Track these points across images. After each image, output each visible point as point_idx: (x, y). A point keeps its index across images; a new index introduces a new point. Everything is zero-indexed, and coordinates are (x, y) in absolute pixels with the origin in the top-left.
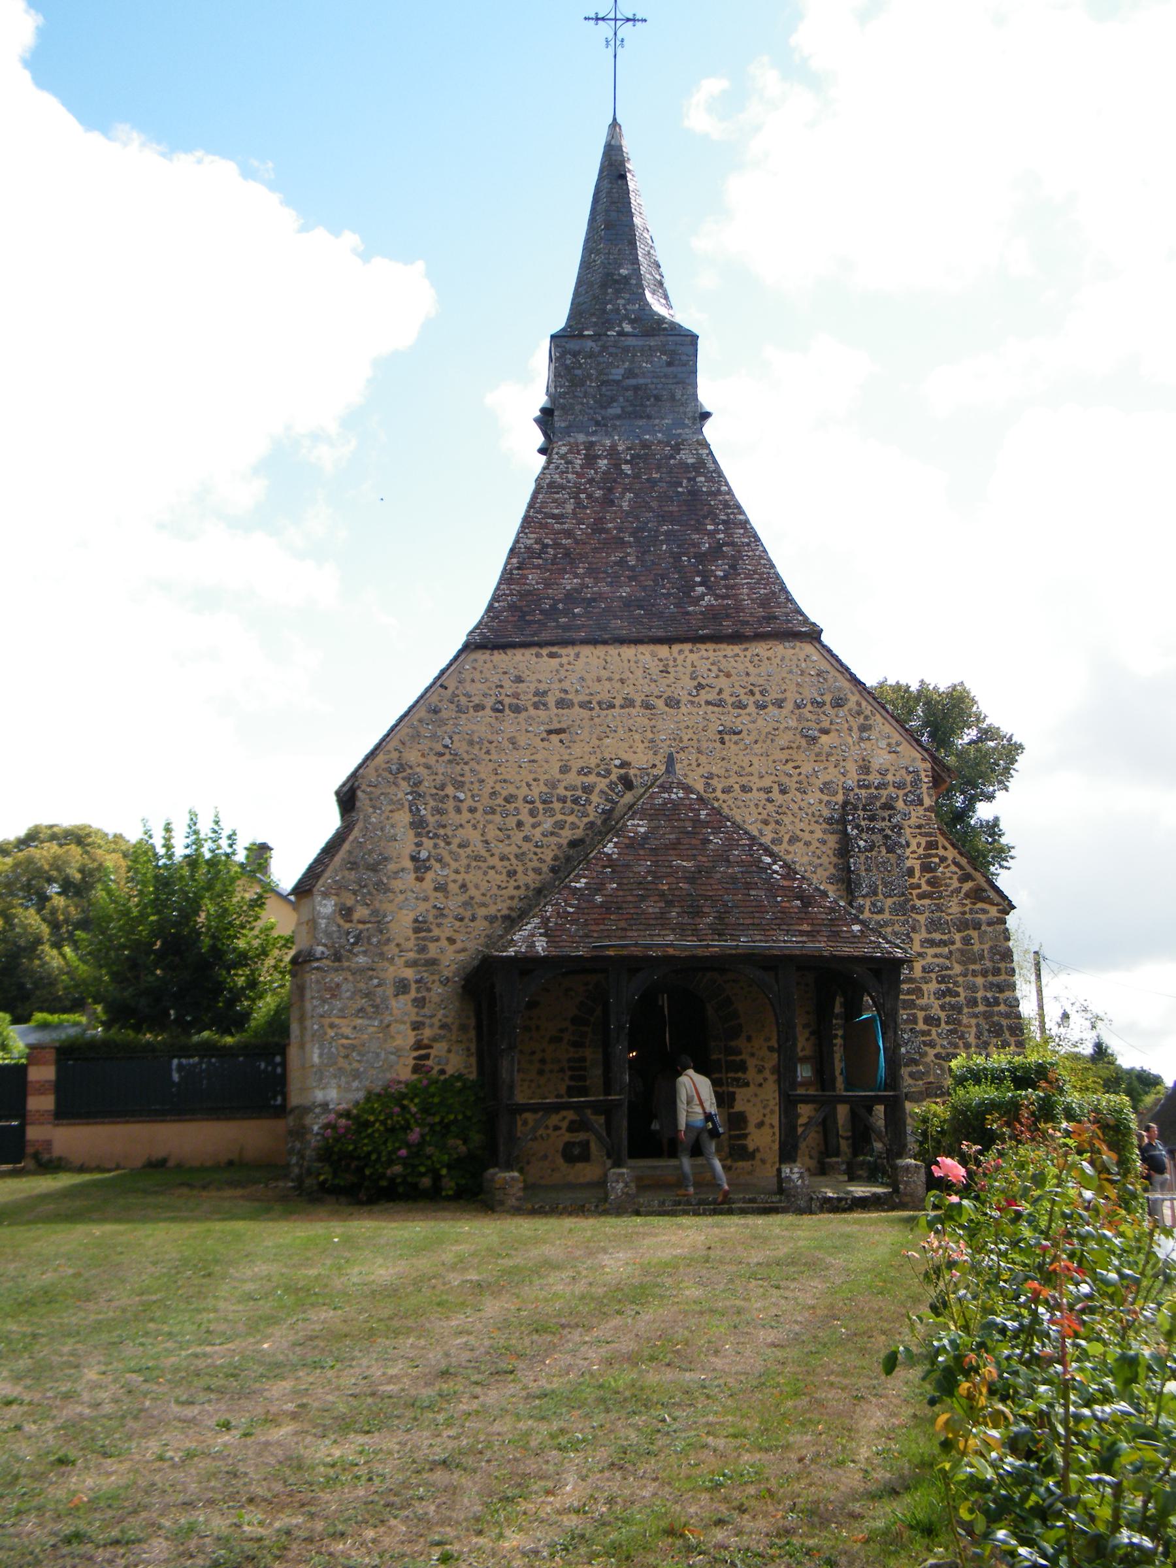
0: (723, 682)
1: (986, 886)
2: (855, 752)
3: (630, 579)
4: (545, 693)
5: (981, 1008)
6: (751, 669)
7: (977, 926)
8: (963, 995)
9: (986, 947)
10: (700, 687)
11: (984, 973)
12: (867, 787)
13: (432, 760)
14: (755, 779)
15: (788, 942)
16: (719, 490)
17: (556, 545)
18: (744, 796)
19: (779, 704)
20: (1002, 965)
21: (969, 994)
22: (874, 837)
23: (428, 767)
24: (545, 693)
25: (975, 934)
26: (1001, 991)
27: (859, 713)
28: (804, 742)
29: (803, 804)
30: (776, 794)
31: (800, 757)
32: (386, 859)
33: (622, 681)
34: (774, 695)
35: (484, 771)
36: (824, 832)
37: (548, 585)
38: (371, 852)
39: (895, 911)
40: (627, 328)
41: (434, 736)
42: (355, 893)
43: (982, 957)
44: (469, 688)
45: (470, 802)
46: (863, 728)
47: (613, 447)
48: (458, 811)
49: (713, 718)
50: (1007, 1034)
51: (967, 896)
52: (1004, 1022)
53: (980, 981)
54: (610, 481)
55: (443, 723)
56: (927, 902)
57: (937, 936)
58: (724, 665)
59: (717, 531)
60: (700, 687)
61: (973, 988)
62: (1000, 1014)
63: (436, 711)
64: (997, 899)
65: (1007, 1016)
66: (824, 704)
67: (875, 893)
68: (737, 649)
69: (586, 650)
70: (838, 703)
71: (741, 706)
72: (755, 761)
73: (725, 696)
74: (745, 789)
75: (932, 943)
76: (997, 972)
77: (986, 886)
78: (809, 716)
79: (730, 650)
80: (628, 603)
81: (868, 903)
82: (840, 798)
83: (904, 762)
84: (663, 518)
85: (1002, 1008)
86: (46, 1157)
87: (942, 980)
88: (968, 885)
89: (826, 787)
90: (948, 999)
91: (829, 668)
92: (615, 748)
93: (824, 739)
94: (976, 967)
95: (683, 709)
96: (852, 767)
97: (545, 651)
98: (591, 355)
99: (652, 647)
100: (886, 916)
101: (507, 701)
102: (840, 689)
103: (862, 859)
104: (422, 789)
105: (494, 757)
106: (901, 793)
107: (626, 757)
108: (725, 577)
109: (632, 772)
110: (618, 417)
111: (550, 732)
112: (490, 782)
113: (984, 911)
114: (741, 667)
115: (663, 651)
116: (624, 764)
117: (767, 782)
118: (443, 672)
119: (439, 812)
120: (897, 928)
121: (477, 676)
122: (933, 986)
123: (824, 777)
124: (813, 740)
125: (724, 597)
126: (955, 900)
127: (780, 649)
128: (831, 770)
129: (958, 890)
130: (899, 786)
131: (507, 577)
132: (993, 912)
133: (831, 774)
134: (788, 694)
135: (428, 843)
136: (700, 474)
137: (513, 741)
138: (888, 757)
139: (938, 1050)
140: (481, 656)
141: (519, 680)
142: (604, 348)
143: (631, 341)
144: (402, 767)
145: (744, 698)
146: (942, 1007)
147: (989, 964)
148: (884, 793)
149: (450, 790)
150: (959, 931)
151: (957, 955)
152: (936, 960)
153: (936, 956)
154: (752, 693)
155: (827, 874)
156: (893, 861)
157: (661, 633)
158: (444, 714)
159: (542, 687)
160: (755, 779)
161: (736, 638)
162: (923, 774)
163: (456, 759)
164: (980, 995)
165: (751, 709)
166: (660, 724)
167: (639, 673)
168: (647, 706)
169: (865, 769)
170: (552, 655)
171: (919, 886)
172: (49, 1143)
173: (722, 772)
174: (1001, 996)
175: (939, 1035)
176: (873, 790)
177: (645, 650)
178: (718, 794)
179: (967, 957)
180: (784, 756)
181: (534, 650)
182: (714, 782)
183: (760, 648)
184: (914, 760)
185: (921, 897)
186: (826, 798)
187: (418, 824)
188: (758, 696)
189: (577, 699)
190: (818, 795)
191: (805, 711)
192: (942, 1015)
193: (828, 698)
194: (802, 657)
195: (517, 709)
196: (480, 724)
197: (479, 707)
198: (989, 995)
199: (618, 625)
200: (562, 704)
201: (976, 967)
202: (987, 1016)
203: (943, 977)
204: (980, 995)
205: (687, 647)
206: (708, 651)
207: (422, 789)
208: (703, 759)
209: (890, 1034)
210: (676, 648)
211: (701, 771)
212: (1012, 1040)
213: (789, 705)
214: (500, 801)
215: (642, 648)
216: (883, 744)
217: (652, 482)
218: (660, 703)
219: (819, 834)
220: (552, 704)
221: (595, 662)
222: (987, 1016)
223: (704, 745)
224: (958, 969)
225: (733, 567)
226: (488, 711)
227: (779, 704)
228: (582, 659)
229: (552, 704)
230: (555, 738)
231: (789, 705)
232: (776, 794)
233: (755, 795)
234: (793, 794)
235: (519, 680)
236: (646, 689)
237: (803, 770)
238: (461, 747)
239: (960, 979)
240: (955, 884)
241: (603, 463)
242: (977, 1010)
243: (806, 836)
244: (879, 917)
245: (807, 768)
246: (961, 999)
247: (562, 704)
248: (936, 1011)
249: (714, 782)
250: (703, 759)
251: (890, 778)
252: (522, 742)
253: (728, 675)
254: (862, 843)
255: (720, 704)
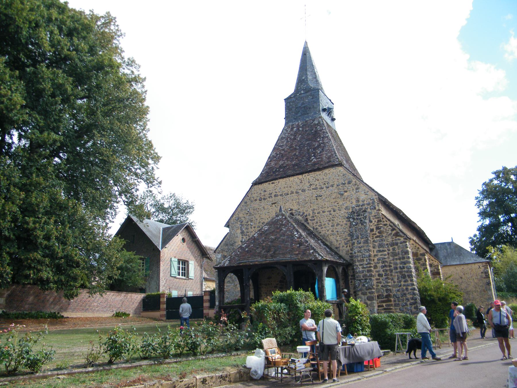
0: (317, 182)
1: (399, 231)
2: (355, 196)
3: (296, 158)
4: (271, 194)
5: (399, 270)
6: (324, 177)
7: (397, 244)
8: (393, 266)
9: (400, 251)
10: (311, 185)
11: (400, 259)
12: (359, 206)
13: (245, 215)
14: (326, 208)
15: (288, 257)
16: (323, 129)
17: (280, 153)
18: (324, 214)
19: (332, 186)
20: (405, 256)
21: (395, 266)
22: (358, 221)
23: (244, 217)
24: (271, 194)
25: (396, 247)
26: (405, 264)
27: (355, 185)
28: (339, 196)
29: (340, 214)
30: (332, 212)
31: (338, 200)
32: (235, 242)
33: (290, 187)
34: (331, 184)
35: (257, 216)
36: (346, 221)
37: (276, 165)
38: (231, 241)
39: (364, 243)
40: (302, 92)
41: (246, 209)
42: (227, 252)
43: (399, 254)
44: (253, 195)
45: (254, 225)
46: (357, 189)
47: (298, 124)
48: (251, 228)
49: (314, 193)
50: (407, 278)
51: (394, 235)
52: (406, 274)
53: (398, 261)
54: (295, 135)
55: (247, 205)
56: (378, 239)
57: (381, 249)
58: (317, 177)
59: (320, 140)
60: (311, 185)
61: (396, 264)
62: (405, 271)
63: (246, 203)
64: (403, 235)
65: (407, 272)
66: (345, 183)
67: (358, 238)
68: (320, 172)
69: (281, 180)
70: (349, 183)
71: (322, 188)
72: (326, 203)
73: (318, 186)
74: (324, 212)
75: (380, 251)
76: (404, 258)
77: (399, 231)
78: (341, 188)
79: (318, 173)
80: (294, 165)
81: (356, 241)
82: (351, 210)
83: (369, 197)
84: (307, 140)
85: (406, 269)
86: (207, 317)
87: (383, 262)
88: (394, 232)
89: (347, 208)
90: (385, 268)
91: (346, 173)
92: (289, 206)
93: (346, 194)
94: (397, 257)
95: (306, 192)
96: (354, 201)
97: (271, 183)
98: (293, 102)
99: (297, 176)
100: (362, 245)
101: (262, 197)
102: (350, 178)
103: (354, 228)
104: (243, 223)
105: (259, 212)
106: (369, 206)
107: (292, 208)
108: (320, 153)
109: (293, 211)
110: (300, 116)
111: (272, 204)
112: (259, 219)
113: (399, 239)
114: (321, 177)
115: (300, 177)
116: (291, 210)
117: (330, 209)
118: (247, 192)
119: (247, 229)
120: (365, 248)
121: (255, 192)
122: (380, 264)
123: (346, 205)
124: (342, 194)
125: (318, 158)
126: (390, 237)
127: (332, 170)
128: (348, 203)
129: (391, 234)
130: (368, 204)
131: (267, 165)
132: (402, 239)
133: (348, 204)
134: (335, 183)
135: (245, 237)
136: (318, 126)
137: (264, 208)
138: (364, 196)
139: (382, 284)
140: (256, 187)
141: (265, 191)
142: (297, 99)
143: (302, 95)
144: (238, 219)
145: (322, 186)
146: (383, 271)
147: (401, 256)
148: (364, 207)
149: (249, 223)
150: (391, 246)
151: (391, 254)
152: (381, 256)
153: (381, 255)
154: (325, 184)
155: (347, 234)
156: (363, 227)
157: (298, 172)
158: (248, 203)
159: (271, 192)
160: (326, 208)
161: (319, 169)
162: (375, 200)
163: (251, 214)
164: (398, 266)
165: (325, 189)
166: (300, 197)
167: (295, 184)
168: (297, 193)
169: (358, 201)
170: (273, 183)
171: (376, 234)
172: (208, 314)
173: (317, 208)
174: (405, 266)
175: (382, 279)
176: (361, 207)
177: (296, 177)
178: (316, 214)
179: (394, 254)
180: (334, 201)
181: (268, 183)
182: (315, 211)
183: (326, 171)
184: (372, 196)
185: (376, 237)
186: (347, 211)
187: (242, 233)
188: (327, 185)
189: (279, 194)
190: (345, 210)
191: (340, 187)
192: (383, 273)
193: (346, 182)
194: (338, 171)
195: (265, 199)
196: (256, 205)
197: (256, 200)
198: (401, 266)
199: (290, 172)
200: (275, 196)
201: (397, 257)
202: (400, 272)
203: (383, 261)
204: (398, 266)
205: (307, 174)
206: (312, 174)
207: (243, 223)
208: (312, 205)
209: (320, 283)
210: (304, 175)
211: (311, 208)
212: (409, 280)
213: (335, 186)
214: (261, 224)
215: (295, 177)
216: (363, 193)
217: (306, 131)
218: (300, 191)
219: (345, 222)
220: (273, 196)
221: (283, 183)
222: (400, 272)
223: (312, 201)
224: (391, 258)
225: (323, 150)
226: (258, 201)
227: (332, 186)
228: (280, 183)
229: (273, 196)
230: (274, 205)
231: (335, 186)
232: (332, 212)
233: (327, 213)
234: (337, 211)
235: (265, 191)
236: (297, 188)
237: (340, 204)
238: (252, 211)
239: (392, 262)
240: (390, 232)
241: (295, 129)
242: (397, 271)
243: (341, 223)
244: (360, 245)
245: (341, 203)
246: (392, 268)
247: (275, 196)
248: (381, 272)
249: (315, 211)
250: (312, 205)
251: (365, 202)
252: (266, 207)
253: (318, 180)
254: (354, 223)
255: (316, 189)
